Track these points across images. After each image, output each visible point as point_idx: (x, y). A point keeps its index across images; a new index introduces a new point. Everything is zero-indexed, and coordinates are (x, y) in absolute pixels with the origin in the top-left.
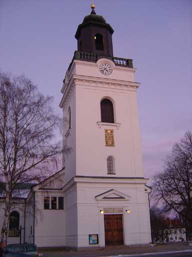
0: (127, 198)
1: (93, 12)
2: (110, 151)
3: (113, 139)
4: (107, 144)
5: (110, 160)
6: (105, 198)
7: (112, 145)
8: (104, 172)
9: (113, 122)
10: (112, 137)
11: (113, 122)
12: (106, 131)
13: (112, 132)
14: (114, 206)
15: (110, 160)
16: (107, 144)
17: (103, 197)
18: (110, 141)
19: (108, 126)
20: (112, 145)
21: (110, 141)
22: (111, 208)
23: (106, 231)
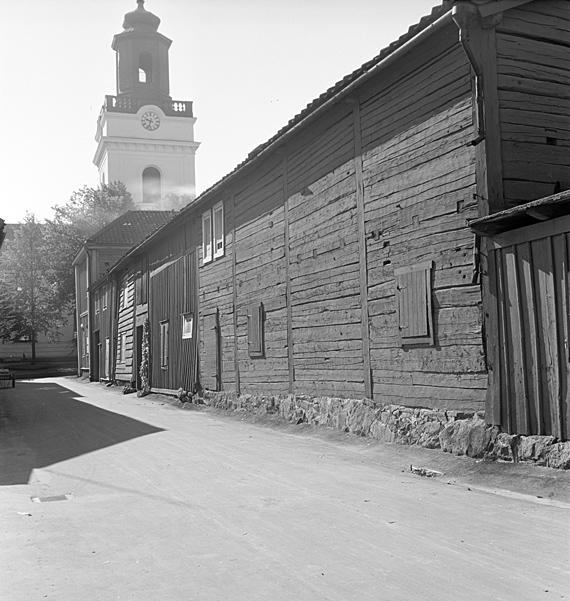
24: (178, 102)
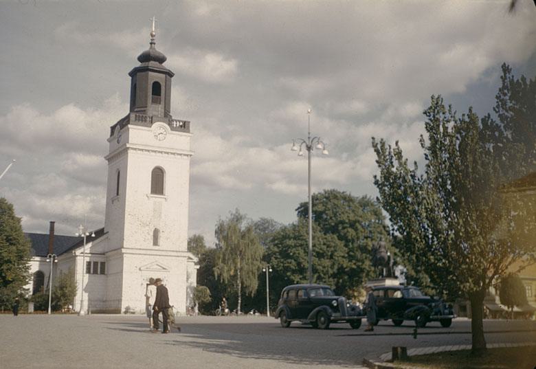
5: (156, 232)
19: (157, 198)
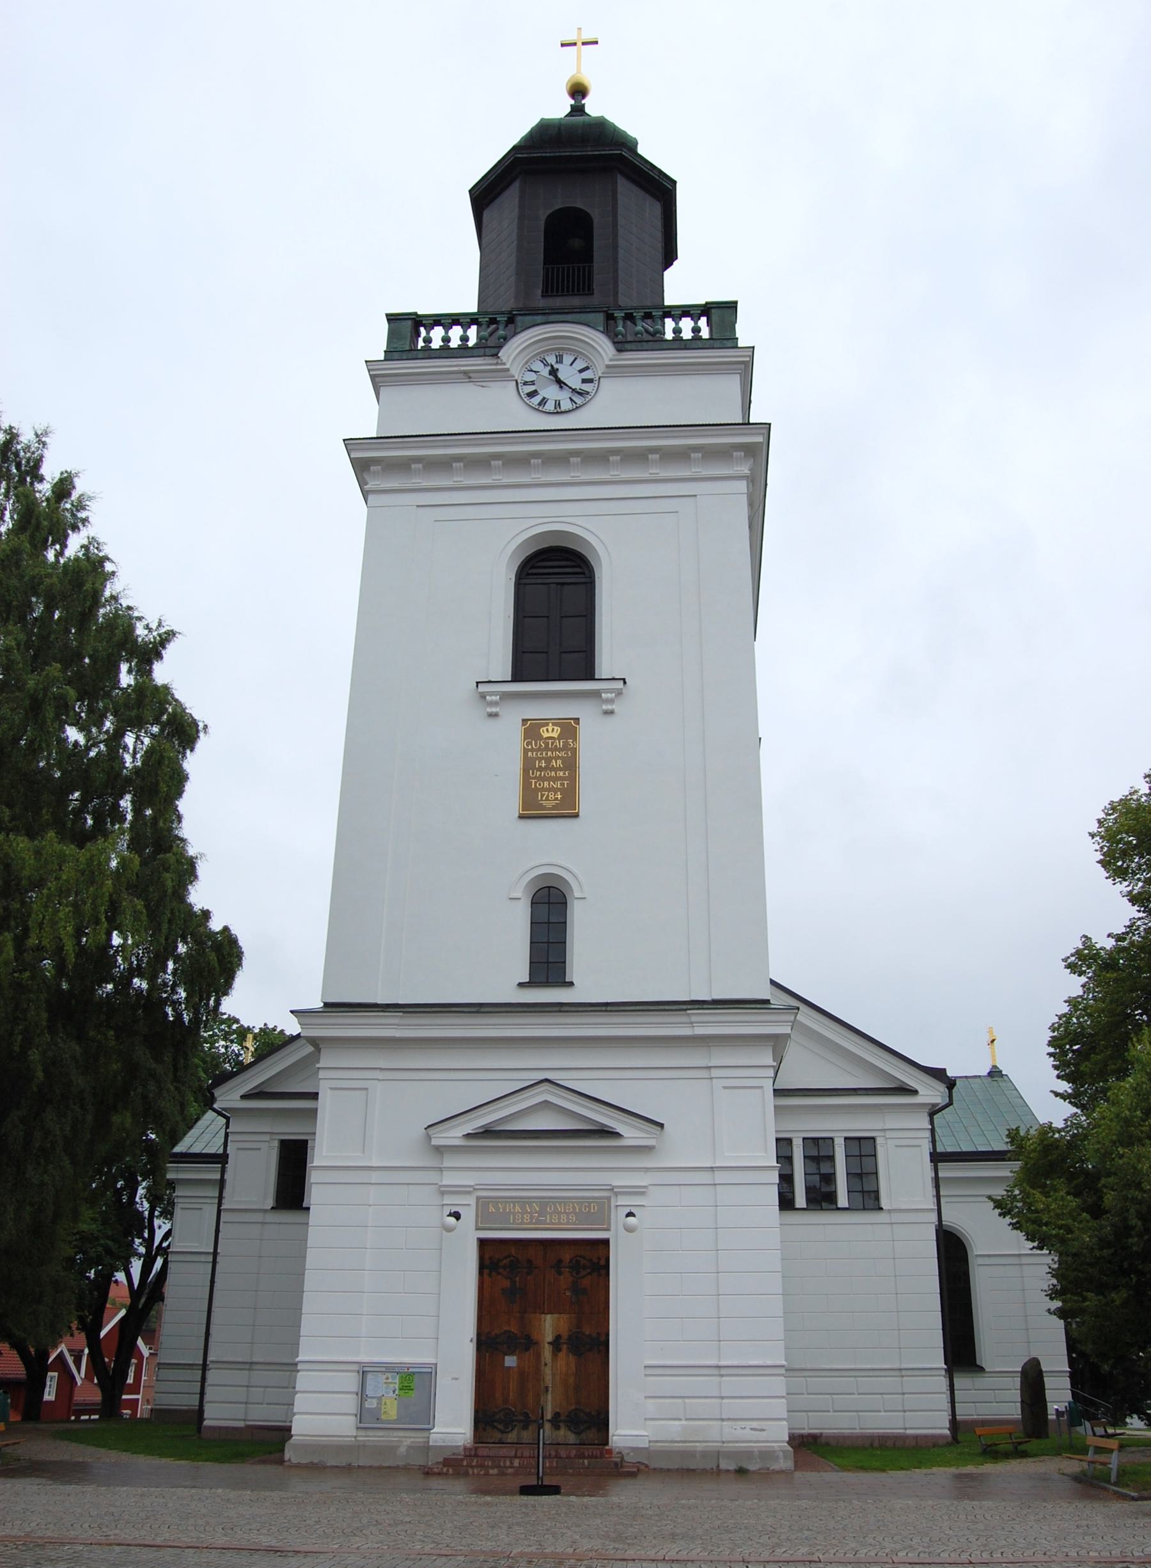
0: (631, 1134)
1: (579, 71)
2: (550, 847)
3: (573, 779)
4: (532, 809)
5: (550, 907)
6: (487, 1133)
7: (567, 809)
8: (504, 971)
9: (283, 1143)
10: (571, 765)
11: (588, 672)
12: (532, 729)
13: (569, 728)
14: (544, 1189)
15: (550, 907)
16: (532, 809)
17: (469, 1128)
18: (549, 787)
19: (552, 702)
20: (567, 809)
21: (549, 787)
22: (523, 1202)
23: (488, 1345)
24: (437, 320)
